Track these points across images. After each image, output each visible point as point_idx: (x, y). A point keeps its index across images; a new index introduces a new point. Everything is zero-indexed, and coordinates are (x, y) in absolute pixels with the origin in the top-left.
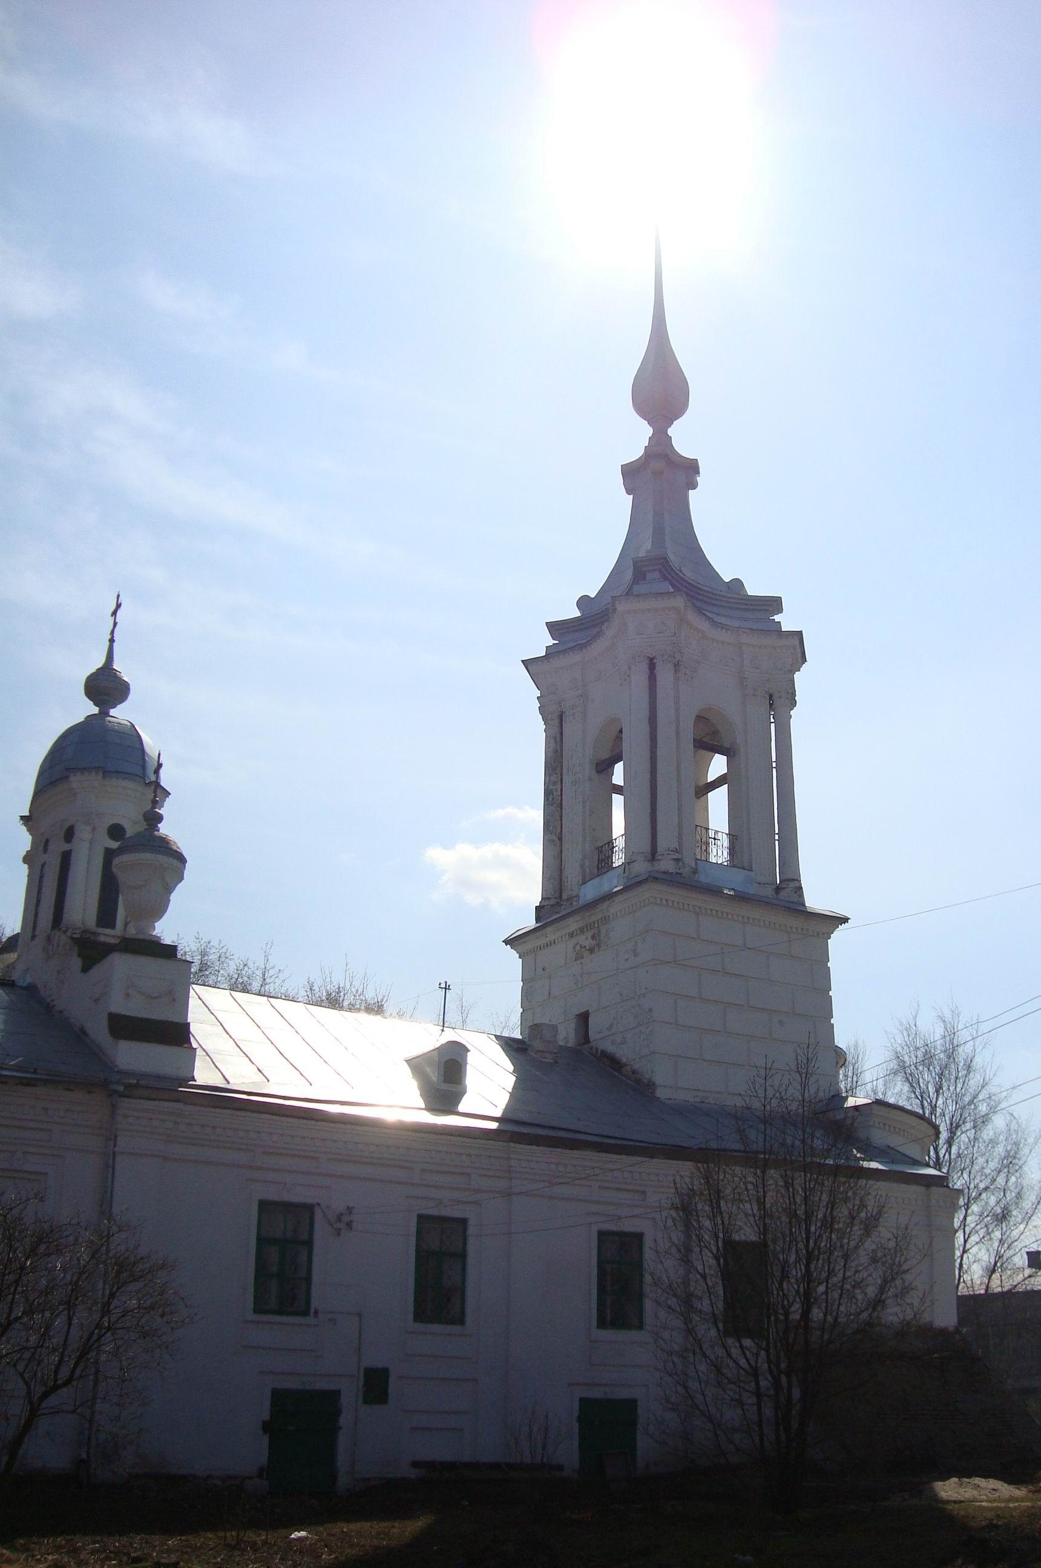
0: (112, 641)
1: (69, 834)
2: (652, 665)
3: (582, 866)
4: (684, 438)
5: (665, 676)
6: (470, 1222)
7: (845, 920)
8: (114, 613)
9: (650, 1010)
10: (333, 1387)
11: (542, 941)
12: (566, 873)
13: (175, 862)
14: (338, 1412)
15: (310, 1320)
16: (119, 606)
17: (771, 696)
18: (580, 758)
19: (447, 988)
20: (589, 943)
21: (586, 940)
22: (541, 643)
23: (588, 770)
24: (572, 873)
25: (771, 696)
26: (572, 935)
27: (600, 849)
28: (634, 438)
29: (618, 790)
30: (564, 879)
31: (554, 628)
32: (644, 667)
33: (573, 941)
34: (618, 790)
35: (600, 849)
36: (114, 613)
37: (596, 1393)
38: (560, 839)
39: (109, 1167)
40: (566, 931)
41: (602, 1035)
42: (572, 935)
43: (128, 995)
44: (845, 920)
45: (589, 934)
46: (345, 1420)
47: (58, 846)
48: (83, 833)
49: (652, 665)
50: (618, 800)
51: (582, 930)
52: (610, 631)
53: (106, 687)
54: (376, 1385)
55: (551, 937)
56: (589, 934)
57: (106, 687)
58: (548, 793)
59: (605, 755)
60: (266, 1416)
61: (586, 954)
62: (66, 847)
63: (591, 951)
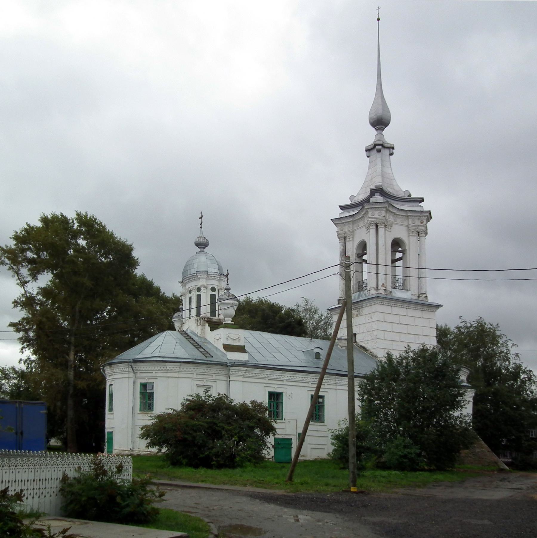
1: (199, 290)
4: (389, 135)
5: (381, 230)
7: (442, 306)
14: (292, 444)
16: (202, 217)
18: (352, 250)
28: (370, 135)
32: (375, 227)
36: (202, 223)
44: (442, 306)
49: (377, 226)
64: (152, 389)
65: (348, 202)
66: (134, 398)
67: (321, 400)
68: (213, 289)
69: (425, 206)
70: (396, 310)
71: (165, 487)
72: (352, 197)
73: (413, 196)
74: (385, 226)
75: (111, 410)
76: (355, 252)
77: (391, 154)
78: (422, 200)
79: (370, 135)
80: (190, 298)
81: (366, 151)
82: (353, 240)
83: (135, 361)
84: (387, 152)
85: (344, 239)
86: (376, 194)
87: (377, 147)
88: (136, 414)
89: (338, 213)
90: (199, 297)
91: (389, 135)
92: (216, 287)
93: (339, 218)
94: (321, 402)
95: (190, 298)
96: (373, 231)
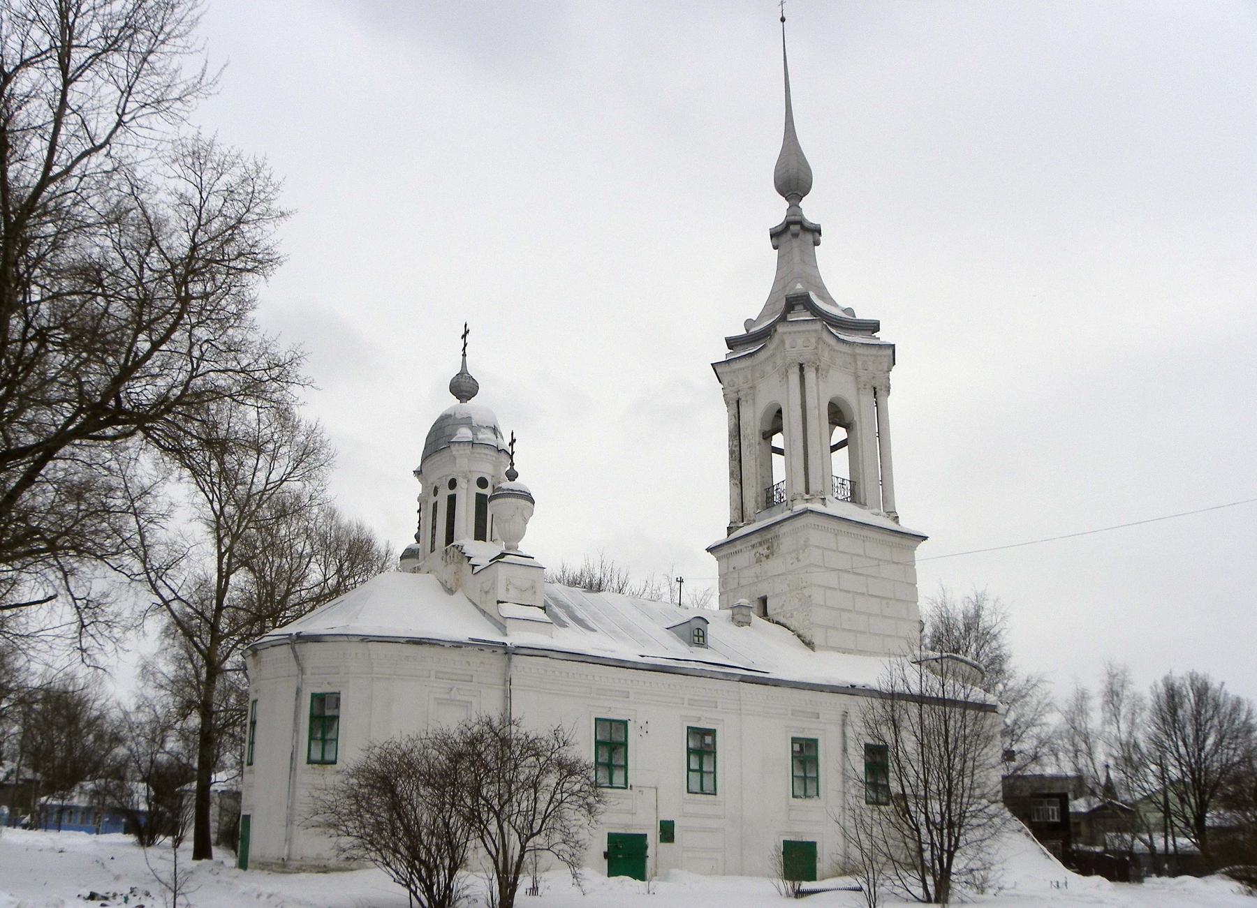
0: (464, 355)
1: (453, 484)
4: (810, 209)
5: (810, 375)
6: (191, 854)
7: (925, 538)
8: (464, 336)
10: (643, 832)
13: (529, 504)
14: (646, 847)
15: (628, 791)
16: (467, 332)
18: (753, 420)
19: (681, 581)
20: (766, 552)
21: (763, 550)
22: (721, 352)
23: (757, 437)
24: (750, 505)
26: (753, 546)
27: (767, 490)
28: (778, 210)
29: (780, 451)
31: (732, 343)
32: (796, 369)
34: (780, 451)
35: (767, 490)
36: (464, 336)
37: (792, 838)
39: (508, 697)
42: (753, 546)
44: (925, 538)
46: (650, 852)
47: (445, 492)
48: (461, 483)
50: (777, 460)
51: (760, 544)
52: (773, 345)
53: (463, 388)
54: (667, 832)
55: (739, 547)
57: (463, 388)
58: (731, 453)
59: (768, 428)
61: (764, 559)
62: (451, 492)
63: (767, 557)
64: (337, 706)
65: (742, 331)
66: (296, 730)
67: (708, 739)
68: (482, 483)
69: (883, 336)
70: (845, 543)
71: (811, 402)
72: (749, 323)
73: (860, 315)
74: (817, 370)
76: (758, 427)
77: (817, 243)
78: (874, 327)
79: (778, 210)
80: (435, 506)
81: (772, 236)
83: (301, 638)
84: (809, 238)
85: (736, 404)
86: (797, 308)
87: (792, 227)
88: (299, 772)
89: (722, 353)
90: (452, 500)
91: (810, 209)
92: (488, 478)
93: (727, 362)
94: (708, 745)
95: (435, 506)
96: (794, 378)
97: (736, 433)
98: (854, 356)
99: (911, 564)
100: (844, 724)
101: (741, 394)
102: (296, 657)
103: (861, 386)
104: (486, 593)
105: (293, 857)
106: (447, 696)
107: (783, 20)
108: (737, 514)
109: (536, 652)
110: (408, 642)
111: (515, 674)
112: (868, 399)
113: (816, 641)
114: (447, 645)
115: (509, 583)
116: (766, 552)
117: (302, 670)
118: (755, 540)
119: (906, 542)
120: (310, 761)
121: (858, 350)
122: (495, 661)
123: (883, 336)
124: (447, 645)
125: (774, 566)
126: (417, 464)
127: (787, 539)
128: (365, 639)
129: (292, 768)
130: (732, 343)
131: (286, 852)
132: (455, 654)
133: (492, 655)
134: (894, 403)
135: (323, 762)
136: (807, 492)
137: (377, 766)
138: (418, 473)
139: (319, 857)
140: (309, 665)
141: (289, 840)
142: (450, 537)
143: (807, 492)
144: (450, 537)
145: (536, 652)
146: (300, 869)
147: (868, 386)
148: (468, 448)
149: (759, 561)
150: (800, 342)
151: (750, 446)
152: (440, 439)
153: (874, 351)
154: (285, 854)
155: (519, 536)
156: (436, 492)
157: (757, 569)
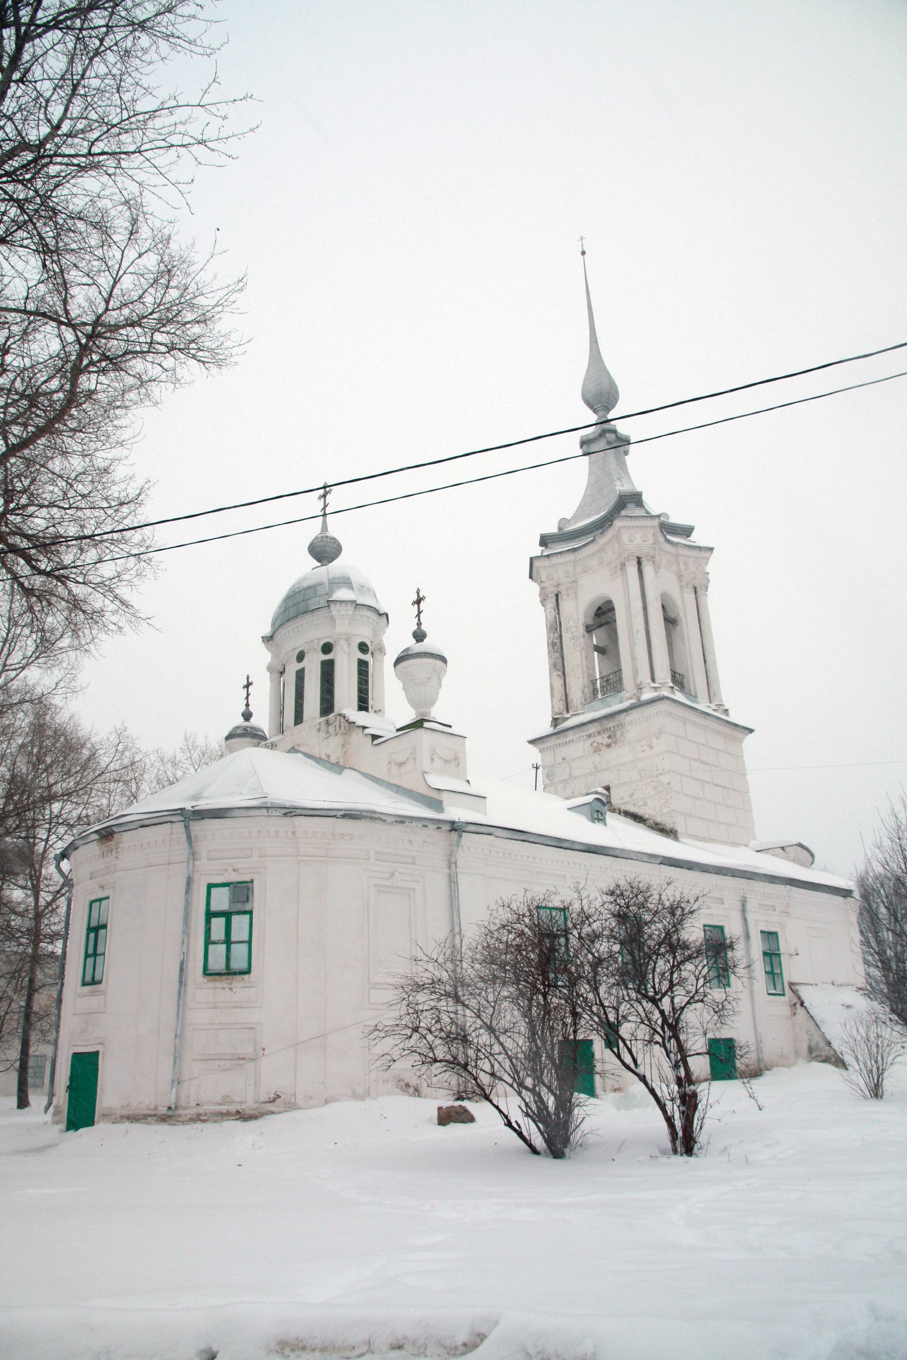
1: (327, 648)
2: (639, 563)
3: (583, 692)
5: (648, 569)
7: (751, 731)
9: (669, 783)
11: (558, 742)
12: (570, 697)
13: (439, 663)
17: (695, 588)
20: (606, 741)
21: (603, 739)
25: (695, 588)
26: (589, 736)
30: (569, 700)
31: (545, 541)
32: (635, 562)
33: (591, 740)
38: (564, 674)
40: (585, 733)
41: (623, 801)
42: (589, 736)
43: (432, 760)
44: (751, 731)
45: (606, 735)
47: (293, 667)
49: (639, 563)
51: (599, 733)
56: (606, 735)
57: (325, 550)
58: (296, 685)
60: (68, 1083)
62: (300, 666)
63: (609, 746)
65: (553, 529)
69: (697, 538)
72: (563, 522)
75: (91, 981)
78: (687, 531)
80: (300, 676)
82: (576, 598)
85: (554, 599)
86: (629, 505)
87: (608, 435)
88: (190, 987)
95: (300, 676)
96: (632, 570)
97: (556, 628)
98: (677, 556)
99: (738, 757)
100: (744, 911)
101: (562, 588)
102: (189, 837)
103: (684, 584)
104: (401, 765)
105: (183, 1102)
106: (388, 883)
107: (583, 253)
108: (561, 706)
109: (483, 829)
110: (344, 816)
111: (462, 857)
112: (690, 597)
113: (680, 828)
114: (389, 820)
115: (433, 753)
116: (606, 741)
117: (193, 855)
118: (592, 729)
119: (737, 734)
120: (207, 972)
121: (682, 551)
122: (440, 840)
123: (697, 538)
124: (389, 820)
125: (615, 755)
126: (267, 630)
127: (635, 726)
128: (291, 812)
129: (182, 982)
130: (545, 541)
131: (173, 1098)
132: (397, 831)
133: (437, 833)
134: (713, 600)
135: (229, 972)
136: (653, 680)
137: (728, 941)
138: (268, 640)
139: (226, 1100)
140: (203, 847)
141: (177, 1081)
142: (327, 706)
143: (653, 680)
144: (327, 706)
145: (483, 829)
146: (198, 1118)
147: (690, 586)
148: (350, 609)
149: (597, 750)
150: (638, 538)
151: (573, 638)
152: (299, 605)
153: (694, 553)
154: (171, 1100)
155: (433, 702)
156: (301, 657)
157: (596, 758)
